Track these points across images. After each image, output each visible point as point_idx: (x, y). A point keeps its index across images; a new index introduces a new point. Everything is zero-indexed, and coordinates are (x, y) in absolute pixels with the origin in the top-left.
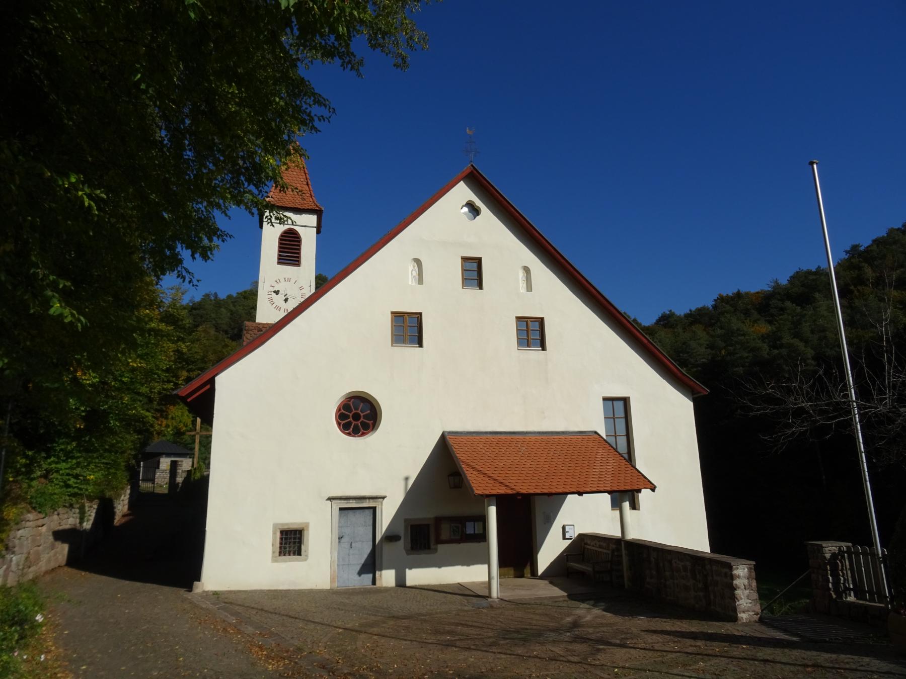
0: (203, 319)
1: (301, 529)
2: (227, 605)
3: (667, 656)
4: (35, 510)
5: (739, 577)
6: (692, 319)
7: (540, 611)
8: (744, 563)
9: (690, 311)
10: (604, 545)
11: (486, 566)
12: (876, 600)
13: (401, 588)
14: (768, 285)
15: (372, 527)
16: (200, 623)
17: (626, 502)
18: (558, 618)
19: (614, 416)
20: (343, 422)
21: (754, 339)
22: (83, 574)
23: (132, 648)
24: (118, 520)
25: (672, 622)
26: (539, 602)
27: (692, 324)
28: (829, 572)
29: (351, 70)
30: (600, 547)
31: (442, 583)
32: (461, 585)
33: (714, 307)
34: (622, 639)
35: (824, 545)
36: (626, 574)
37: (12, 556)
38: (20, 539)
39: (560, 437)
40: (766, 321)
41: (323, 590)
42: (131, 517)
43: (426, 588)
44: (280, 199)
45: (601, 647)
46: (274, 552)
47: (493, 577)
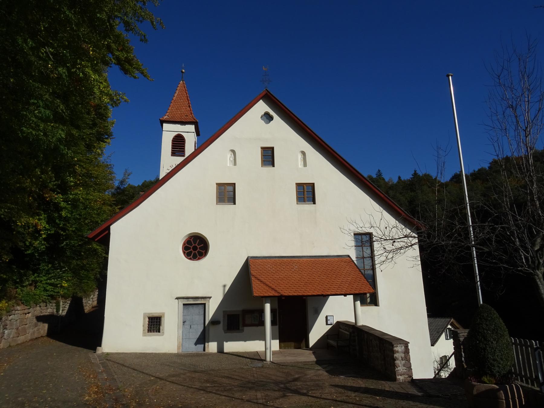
4: (24, 304)
5: (398, 352)
6: (474, 177)
9: (474, 171)
11: (264, 342)
17: (357, 301)
20: (187, 252)
28: (462, 350)
31: (247, 351)
35: (458, 332)
37: (5, 330)
38: (10, 321)
39: (323, 259)
41: (172, 353)
43: (235, 354)
46: (144, 330)
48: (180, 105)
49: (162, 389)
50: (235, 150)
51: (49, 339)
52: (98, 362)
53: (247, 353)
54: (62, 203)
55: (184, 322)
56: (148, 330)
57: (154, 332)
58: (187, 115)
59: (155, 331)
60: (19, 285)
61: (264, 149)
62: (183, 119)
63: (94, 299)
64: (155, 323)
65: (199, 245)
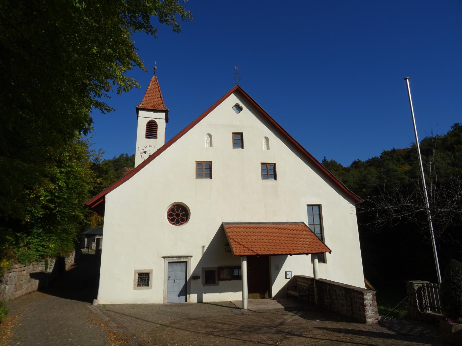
0: (120, 167)
1: (149, 273)
2: (107, 311)
3: (320, 341)
4: (20, 263)
5: (367, 299)
6: (369, 164)
7: (266, 316)
8: (370, 292)
9: (369, 159)
10: (306, 281)
11: (241, 292)
12: (441, 312)
13: (200, 304)
14: (410, 145)
16: (89, 321)
18: (274, 320)
19: (313, 214)
20: (171, 218)
21: (401, 174)
22: (44, 295)
23: (49, 333)
24: (67, 267)
25: (332, 323)
26: (269, 312)
27: (370, 166)
28: (417, 297)
29: (151, 34)
30: (304, 283)
31: (222, 301)
33: (381, 157)
34: (302, 332)
35: (414, 283)
36: (316, 297)
37: (6, 286)
38: (10, 277)
40: (408, 164)
41: (159, 304)
42: (75, 266)
43: (212, 303)
44: (147, 105)
45: (288, 336)
46: (134, 285)
47: (245, 298)
48: (153, 96)
49: (173, 334)
50: (211, 134)
51: (41, 293)
53: (223, 303)
54: (58, 174)
55: (169, 277)
56: (138, 285)
57: (143, 286)
58: (159, 104)
60: (15, 247)
61: (235, 134)
62: (155, 107)
64: (144, 278)
65: (181, 212)
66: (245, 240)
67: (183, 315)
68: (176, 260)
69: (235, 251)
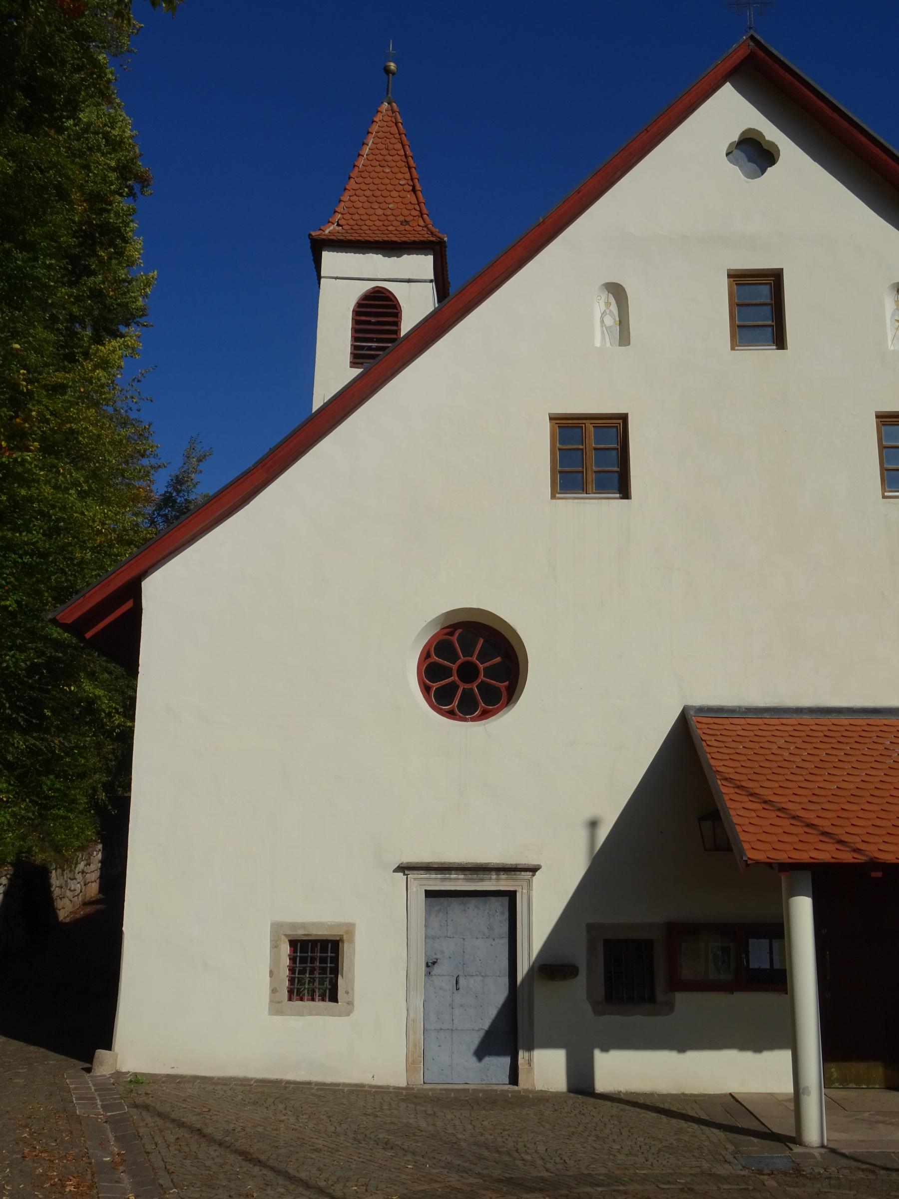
11: (787, 1054)
15: (506, 940)
20: (435, 686)
31: (688, 1092)
32: (737, 1100)
41: (388, 1087)
42: (99, 907)
43: (641, 1101)
44: (356, 227)
46: (274, 991)
52: (98, 1114)
55: (430, 965)
56: (290, 992)
57: (313, 1000)
58: (408, 219)
59: (317, 998)
63: (88, 875)
65: (483, 658)
66: (799, 791)
67: (486, 1154)
68: (460, 883)
69: (734, 809)
